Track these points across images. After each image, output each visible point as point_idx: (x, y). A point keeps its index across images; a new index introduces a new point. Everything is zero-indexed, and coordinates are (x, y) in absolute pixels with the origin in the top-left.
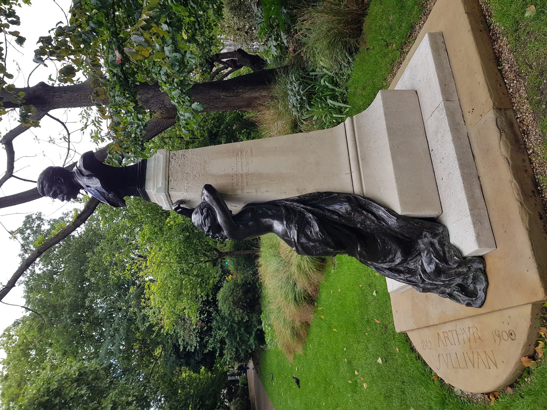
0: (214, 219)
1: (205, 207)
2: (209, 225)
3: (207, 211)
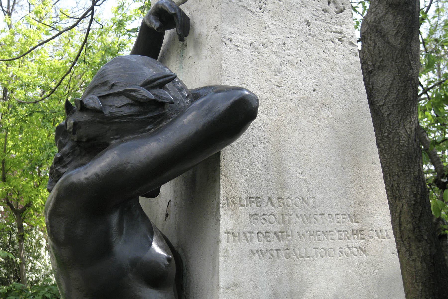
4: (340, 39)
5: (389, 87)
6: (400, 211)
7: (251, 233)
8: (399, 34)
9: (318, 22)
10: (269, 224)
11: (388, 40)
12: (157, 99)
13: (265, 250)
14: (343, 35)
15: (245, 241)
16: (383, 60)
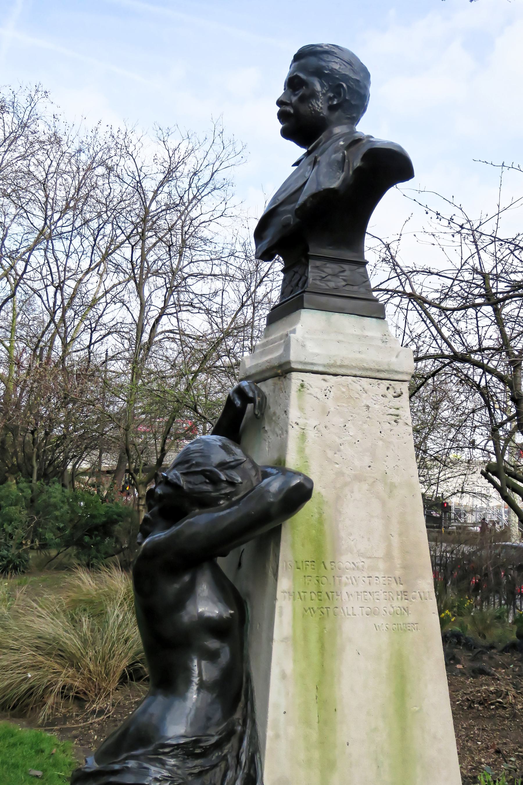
4: (395, 421)
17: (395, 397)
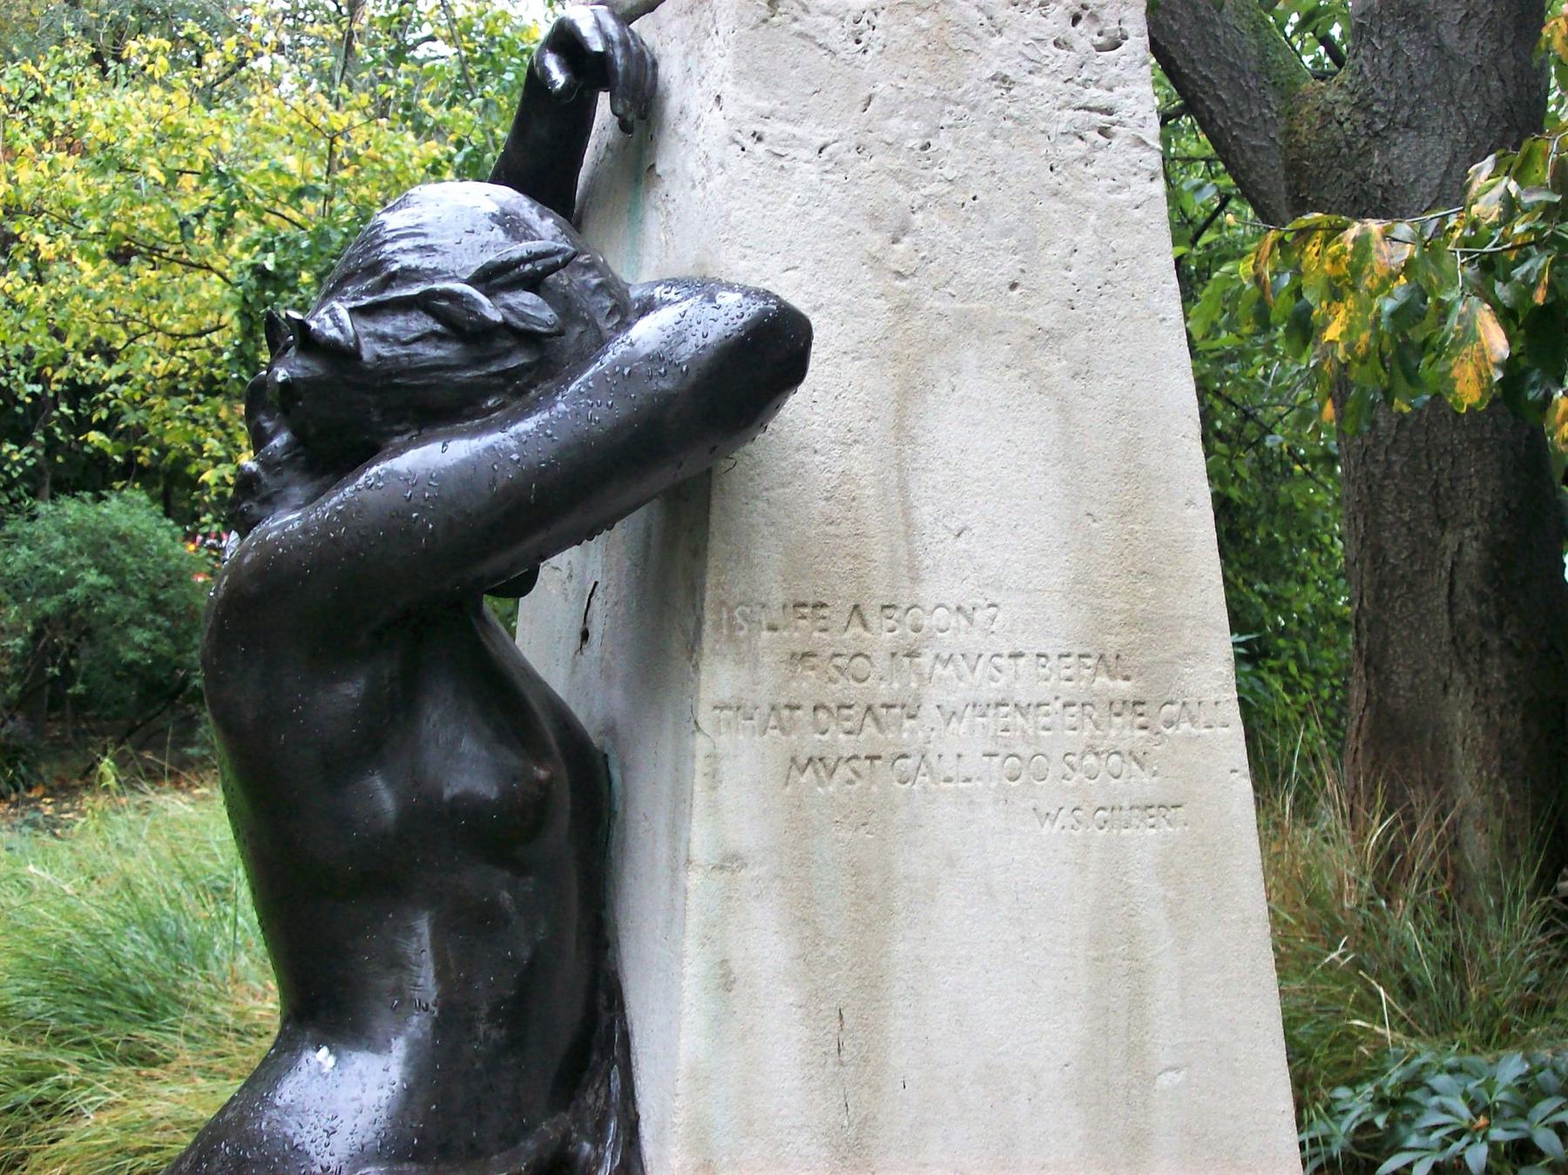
0: (433, 407)
1: (566, 306)
2: (369, 349)
3: (527, 338)
4: (1103, 132)
5: (1437, 181)
6: (1453, 563)
7: (792, 707)
8: (1474, 21)
9: (1038, 81)
10: (852, 682)
11: (1439, 40)
12: (513, 319)
13: (835, 758)
14: (1114, 118)
15: (776, 732)
16: (1421, 101)
17: (1100, 48)
